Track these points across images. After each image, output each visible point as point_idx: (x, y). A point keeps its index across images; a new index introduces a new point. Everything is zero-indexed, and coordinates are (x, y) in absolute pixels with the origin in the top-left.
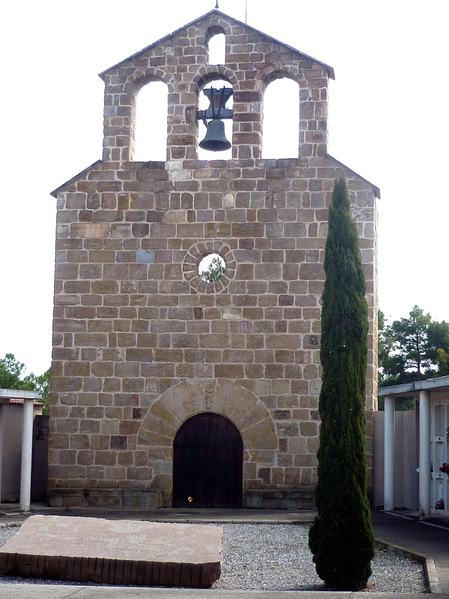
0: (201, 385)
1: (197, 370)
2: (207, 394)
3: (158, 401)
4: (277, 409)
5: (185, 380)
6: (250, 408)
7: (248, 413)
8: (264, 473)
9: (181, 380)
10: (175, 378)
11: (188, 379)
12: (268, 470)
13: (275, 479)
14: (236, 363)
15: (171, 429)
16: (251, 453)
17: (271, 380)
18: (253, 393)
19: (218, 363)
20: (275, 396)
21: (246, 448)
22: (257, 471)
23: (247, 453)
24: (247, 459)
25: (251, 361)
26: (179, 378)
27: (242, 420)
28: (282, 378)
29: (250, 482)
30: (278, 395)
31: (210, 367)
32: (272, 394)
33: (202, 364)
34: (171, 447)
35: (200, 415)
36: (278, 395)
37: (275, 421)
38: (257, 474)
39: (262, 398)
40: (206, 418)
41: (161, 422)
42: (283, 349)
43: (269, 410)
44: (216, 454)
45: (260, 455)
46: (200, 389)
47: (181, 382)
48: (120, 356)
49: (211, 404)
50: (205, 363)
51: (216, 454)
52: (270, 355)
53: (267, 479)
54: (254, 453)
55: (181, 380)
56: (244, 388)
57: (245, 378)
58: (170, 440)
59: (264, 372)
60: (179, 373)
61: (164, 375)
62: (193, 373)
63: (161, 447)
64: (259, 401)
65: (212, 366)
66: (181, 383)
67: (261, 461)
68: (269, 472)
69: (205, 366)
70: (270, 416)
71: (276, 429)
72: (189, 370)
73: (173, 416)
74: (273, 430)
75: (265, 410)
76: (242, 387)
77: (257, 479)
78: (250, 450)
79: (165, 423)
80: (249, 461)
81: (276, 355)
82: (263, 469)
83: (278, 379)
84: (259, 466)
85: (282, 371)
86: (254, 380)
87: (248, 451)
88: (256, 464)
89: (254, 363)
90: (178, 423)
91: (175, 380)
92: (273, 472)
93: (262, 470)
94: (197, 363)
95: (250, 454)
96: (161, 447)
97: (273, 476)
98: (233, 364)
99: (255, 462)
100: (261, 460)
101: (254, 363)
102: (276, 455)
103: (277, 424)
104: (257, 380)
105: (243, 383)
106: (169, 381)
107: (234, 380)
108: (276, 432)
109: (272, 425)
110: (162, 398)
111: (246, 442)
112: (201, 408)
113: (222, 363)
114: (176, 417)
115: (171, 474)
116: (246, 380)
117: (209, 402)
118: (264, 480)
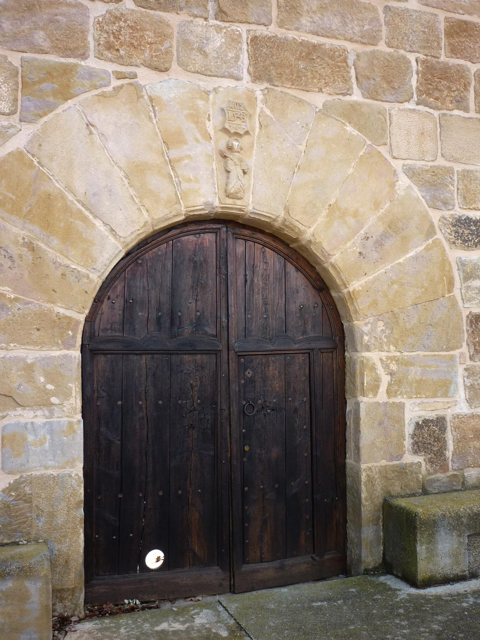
0: (201, 103)
1: (185, 43)
2: (224, 140)
3: (18, 156)
4: (459, 211)
5: (135, 76)
6: (377, 205)
7: (372, 223)
8: (429, 435)
9: (120, 76)
10: (92, 63)
11: (145, 76)
12: (440, 422)
13: (460, 454)
14: (322, 40)
15: (79, 276)
16: (386, 367)
17: (436, 113)
18: (383, 150)
19: (261, 31)
20: (450, 171)
21: (368, 349)
22: (409, 429)
23: (373, 368)
24: (375, 389)
25: (373, 39)
26: (110, 67)
27: (352, 246)
28: (466, 110)
29: (384, 472)
30: (458, 167)
31: (234, 39)
32: (441, 162)
33: (201, 21)
34: (76, 354)
35: (195, 223)
36: (458, 167)
37: (456, 254)
38: (408, 443)
39: (411, 173)
40: (209, 238)
41: (31, 247)
42: (466, 18)
43: (435, 216)
44: (249, 373)
45: (414, 373)
46: (196, 117)
47: (115, 83)
48: (65, 409)
49: (244, 180)
50: (212, 22)
51: (249, 373)
52: (431, 27)
53: (437, 457)
54: (394, 367)
55: (120, 76)
56: (355, 132)
57: (357, 96)
58: (78, 322)
59: (414, 82)
60: (109, 47)
61: (46, 45)
62: (168, 52)
63: (30, 354)
64: (404, 181)
65: (240, 35)
66: (118, 89)
67: (418, 394)
68: (443, 429)
69: (213, 33)
70: (439, 235)
71: (458, 284)
72: (150, 36)
73: (85, 219)
74: (451, 283)
75: (425, 216)
76: (349, 128)
77: (409, 458)
78: (384, 355)
79: (51, 250)
80: (382, 396)
81: (449, 34)
82: (426, 422)
83: (456, 112)
84: (414, 411)
85: (466, 87)
86: (387, 106)
87: (375, 357)
88: (401, 406)
89: (382, 47)
90: (109, 253)
91: (91, 74)
92: (456, 428)
93: (422, 426)
94: (184, 17)
95: (381, 371)
96: (30, 354)
97: (457, 442)
98: (315, 40)
99: (398, 400)
100: (420, 388)
101: (382, 47)
102: (460, 370)
103: (462, 264)
104: (393, 108)
105: (352, 113)
106: (67, 70)
107: (318, 99)
108: (456, 292)
109: (444, 262)
110: (37, 141)
111: (366, 326)
112: (205, 195)
113: (273, 30)
114: (98, 223)
115: (77, 470)
116: (360, 104)
117: (236, 171)
118: (431, 461)
